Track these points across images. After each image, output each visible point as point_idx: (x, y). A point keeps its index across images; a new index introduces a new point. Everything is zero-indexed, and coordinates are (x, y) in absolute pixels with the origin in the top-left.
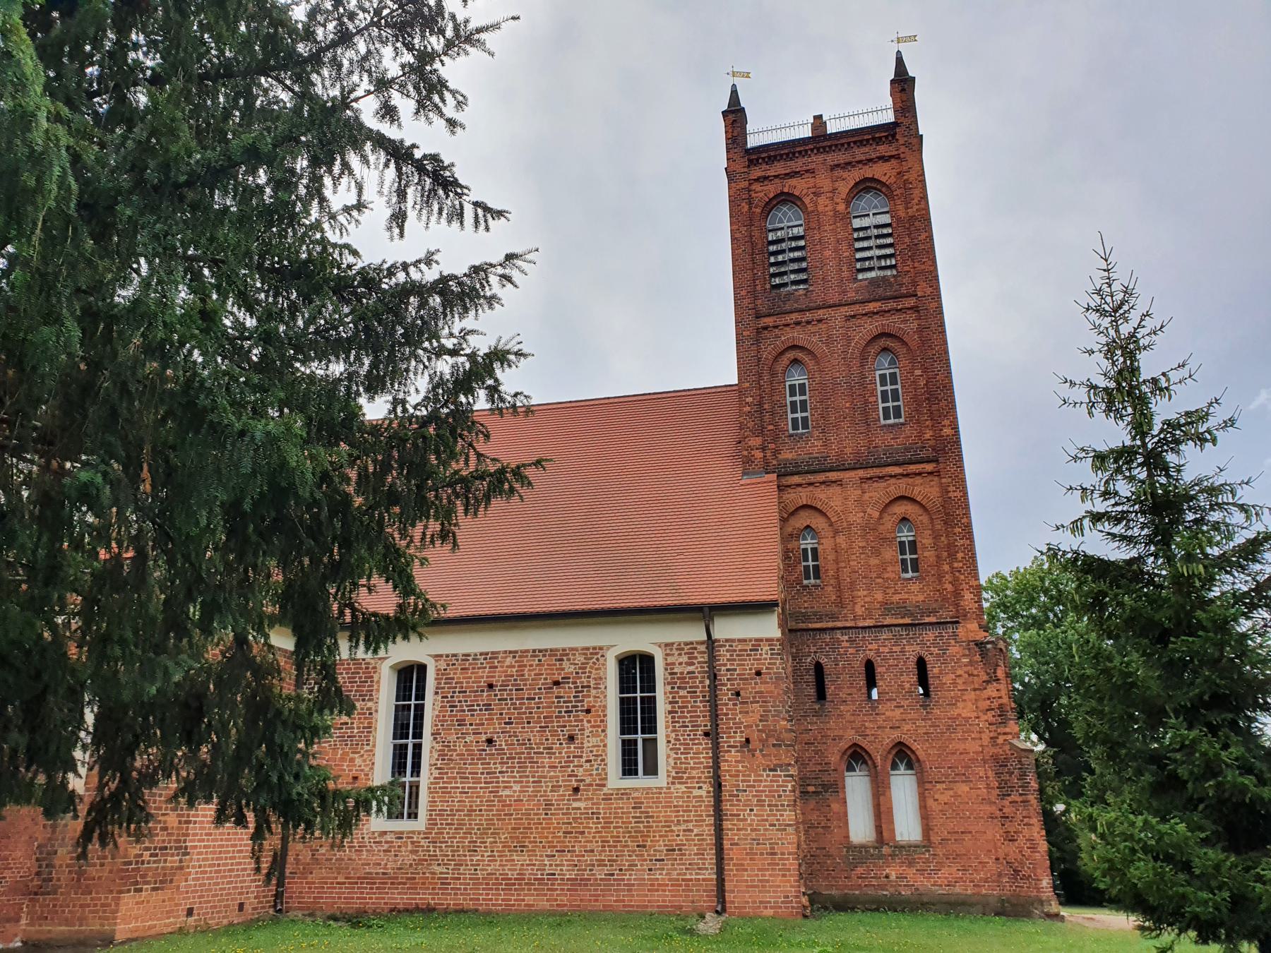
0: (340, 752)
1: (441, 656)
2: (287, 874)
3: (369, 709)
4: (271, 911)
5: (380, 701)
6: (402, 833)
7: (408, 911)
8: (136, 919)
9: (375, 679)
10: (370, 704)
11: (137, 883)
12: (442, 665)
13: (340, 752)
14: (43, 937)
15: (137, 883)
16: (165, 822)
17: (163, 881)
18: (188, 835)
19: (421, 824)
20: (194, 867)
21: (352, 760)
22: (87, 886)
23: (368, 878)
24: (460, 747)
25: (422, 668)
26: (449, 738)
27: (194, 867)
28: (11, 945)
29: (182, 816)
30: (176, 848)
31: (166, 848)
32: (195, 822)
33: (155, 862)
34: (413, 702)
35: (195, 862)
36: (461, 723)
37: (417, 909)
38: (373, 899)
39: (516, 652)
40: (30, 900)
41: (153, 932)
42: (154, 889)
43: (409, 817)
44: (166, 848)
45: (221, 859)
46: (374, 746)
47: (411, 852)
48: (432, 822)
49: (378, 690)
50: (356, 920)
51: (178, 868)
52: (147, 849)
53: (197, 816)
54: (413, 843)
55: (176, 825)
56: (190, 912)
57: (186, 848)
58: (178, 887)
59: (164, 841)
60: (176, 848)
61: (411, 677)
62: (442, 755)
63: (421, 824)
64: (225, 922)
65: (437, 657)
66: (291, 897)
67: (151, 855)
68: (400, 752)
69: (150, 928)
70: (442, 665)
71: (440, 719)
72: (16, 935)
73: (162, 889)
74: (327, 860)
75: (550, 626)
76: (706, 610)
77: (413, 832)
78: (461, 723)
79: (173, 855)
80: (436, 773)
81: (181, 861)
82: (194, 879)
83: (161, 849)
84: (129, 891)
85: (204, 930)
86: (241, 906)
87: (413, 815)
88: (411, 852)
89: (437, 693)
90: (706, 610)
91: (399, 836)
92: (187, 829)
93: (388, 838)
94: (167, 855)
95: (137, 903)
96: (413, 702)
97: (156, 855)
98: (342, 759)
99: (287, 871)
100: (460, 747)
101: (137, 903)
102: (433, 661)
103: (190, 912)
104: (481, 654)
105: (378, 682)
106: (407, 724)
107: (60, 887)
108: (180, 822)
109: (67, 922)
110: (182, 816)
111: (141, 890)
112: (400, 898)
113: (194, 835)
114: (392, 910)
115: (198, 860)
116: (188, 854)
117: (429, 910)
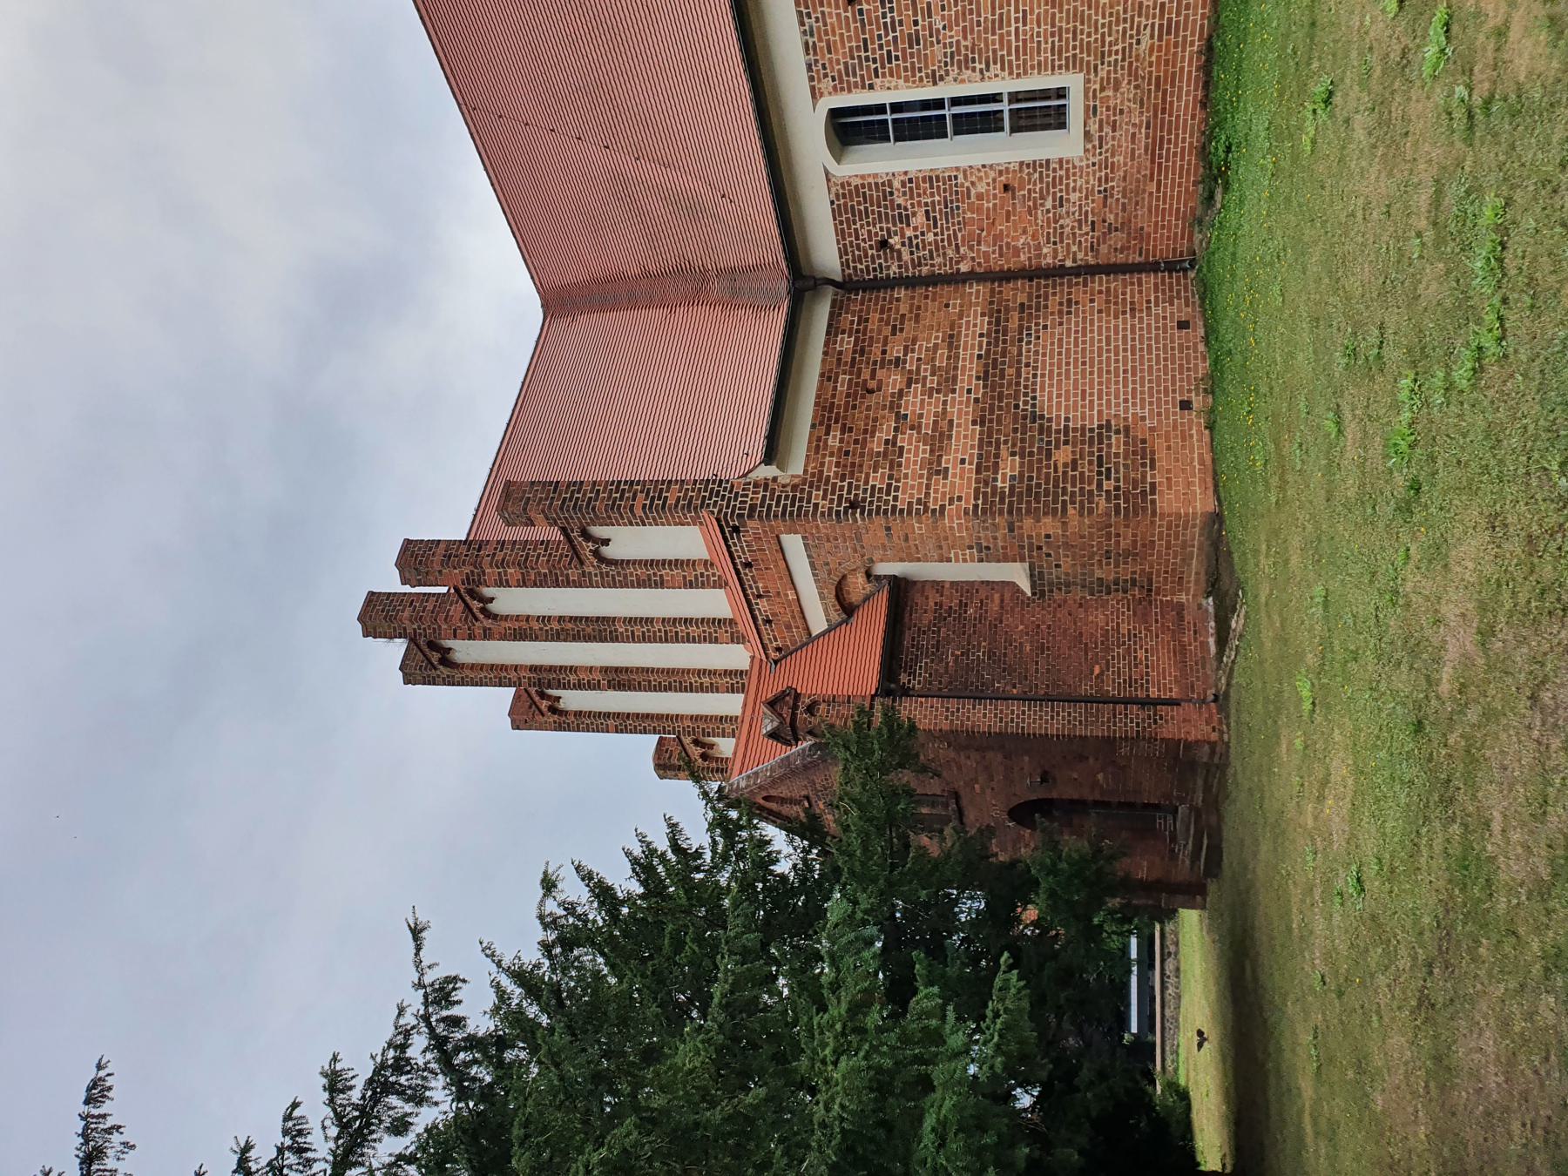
0: (969, 215)
1: (813, 89)
2: (1142, 259)
3: (903, 184)
4: (1192, 274)
5: (891, 171)
6: (1087, 108)
7: (1208, 84)
8: (1189, 484)
9: (859, 182)
10: (896, 184)
11: (1144, 492)
12: (827, 84)
13: (969, 215)
14: (1203, 577)
15: (1144, 492)
16: (1065, 465)
17: (1142, 453)
18: (1083, 427)
19: (1073, 82)
20: (1126, 411)
21: (980, 197)
22: (1144, 545)
23: (1153, 151)
24: (955, 35)
25: (835, 114)
26: (940, 57)
27: (1126, 411)
28: (1211, 610)
29: (1058, 440)
30: (1100, 443)
31: (1100, 457)
32: (1067, 419)
33: (1117, 472)
34: (889, 117)
35: (1120, 409)
36: (914, 40)
37: (1207, 69)
38: (1186, 137)
39: (800, 13)
40: (1158, 594)
41: (1208, 458)
42: (1153, 467)
43: (1064, 97)
44: (1100, 457)
45: (1117, 369)
46: (957, 169)
47: (1116, 89)
48: (1073, 64)
49: (875, 176)
50: (1215, 174)
51: (1127, 436)
52: (1100, 485)
53: (1058, 417)
54: (1103, 89)
55: (1069, 448)
56: (1186, 405)
57: (1100, 427)
58: (1152, 429)
59: (1091, 463)
60: (1100, 443)
61: (849, 129)
62: (966, 63)
63: (1073, 82)
64: (1201, 347)
65: (815, 94)
66: (1175, 250)
67: (1108, 478)
68: (967, 125)
69: (1202, 462)
70: (827, 84)
71: (911, 76)
72: (1200, 606)
73: (1153, 452)
74: (1124, 210)
75: (788, 151)
76: (799, 284)
77: (1086, 91)
78: (914, 40)
79: (1109, 446)
80: (995, 69)
81: (1118, 432)
82: (1143, 408)
83: (1100, 465)
84: (1153, 502)
85: (1213, 384)
86: (1183, 325)
87: (1061, 93)
88: (1116, 89)
89: (871, 87)
90: (799, 284)
91: (1090, 111)
92: (1075, 430)
93: (1094, 128)
94: (1108, 454)
95: (1169, 488)
96: (889, 117)
97: (1109, 469)
98: (979, 210)
99: (1138, 259)
100: (955, 35)
101: (1169, 488)
102: (821, 102)
103: (1186, 405)
104: (802, 24)
105: (863, 177)
106: (920, 124)
107: (1143, 571)
108: (1067, 442)
109: (1186, 560)
110: (1058, 440)
111: (1153, 485)
112: (1186, 97)
113: (1083, 419)
114: (1204, 106)
115: (1118, 405)
116: (1108, 421)
117: (1210, 55)
